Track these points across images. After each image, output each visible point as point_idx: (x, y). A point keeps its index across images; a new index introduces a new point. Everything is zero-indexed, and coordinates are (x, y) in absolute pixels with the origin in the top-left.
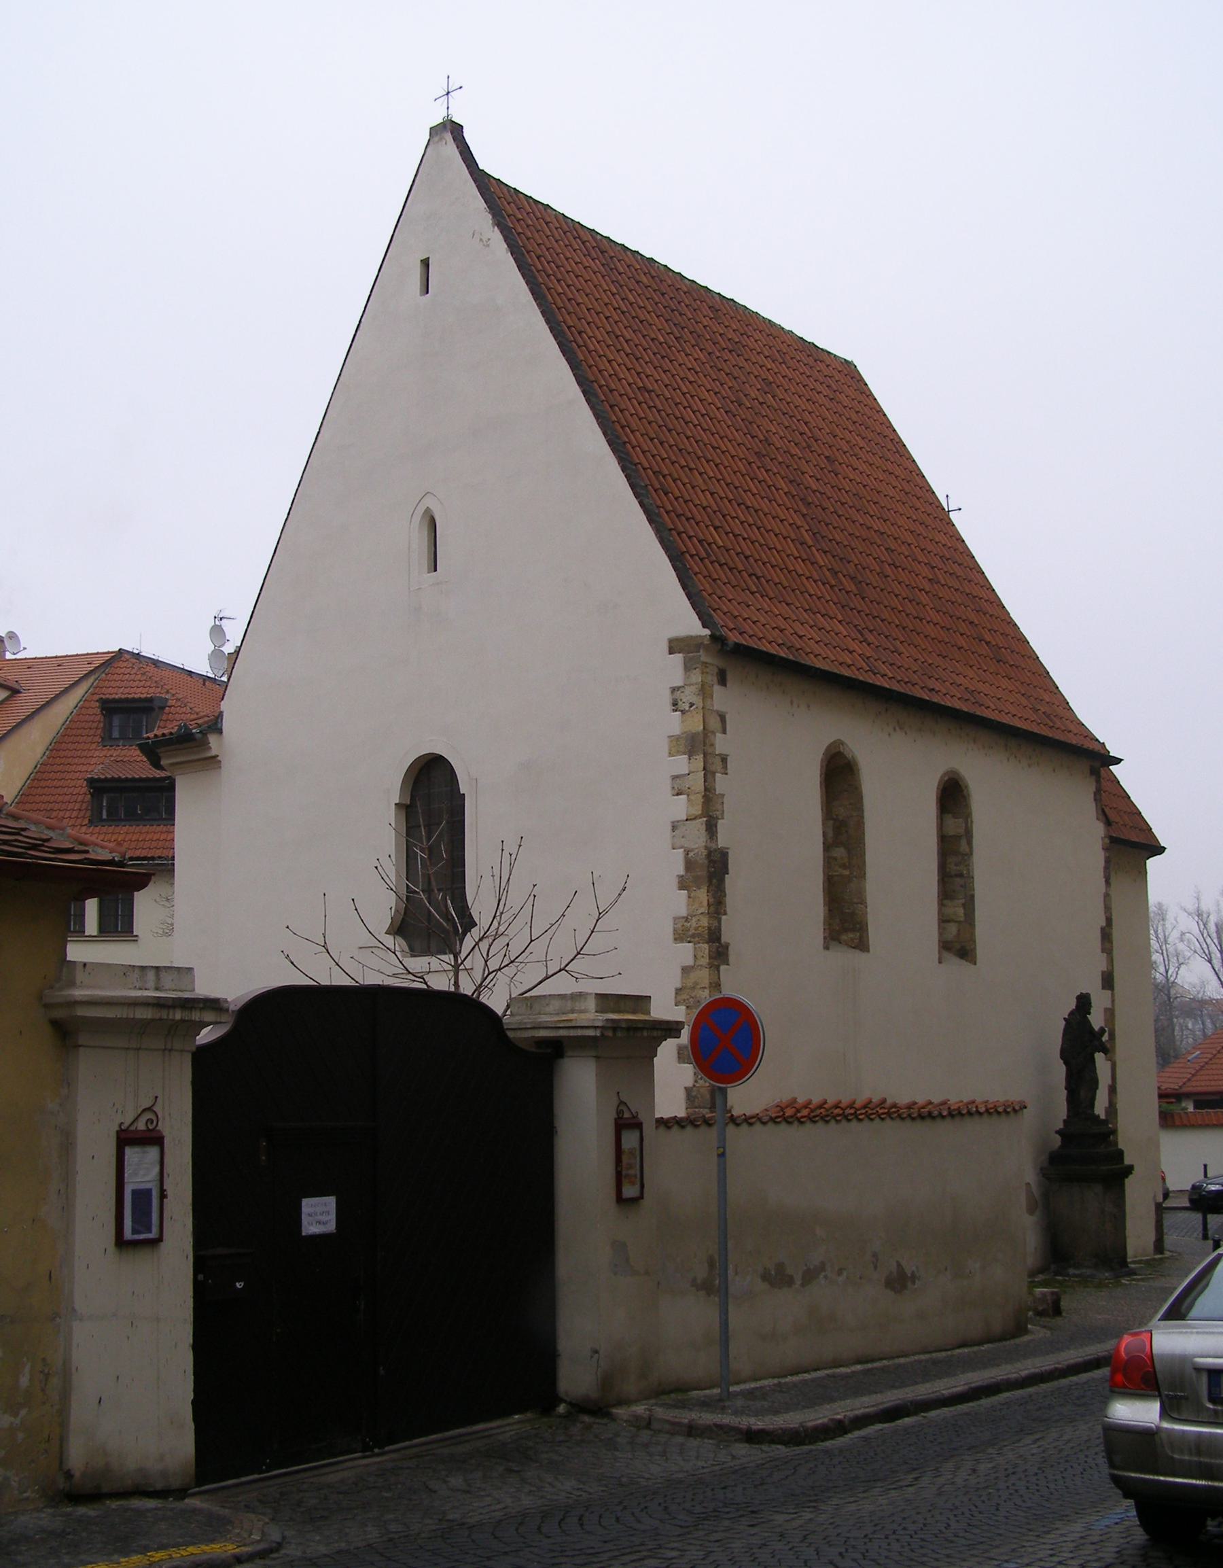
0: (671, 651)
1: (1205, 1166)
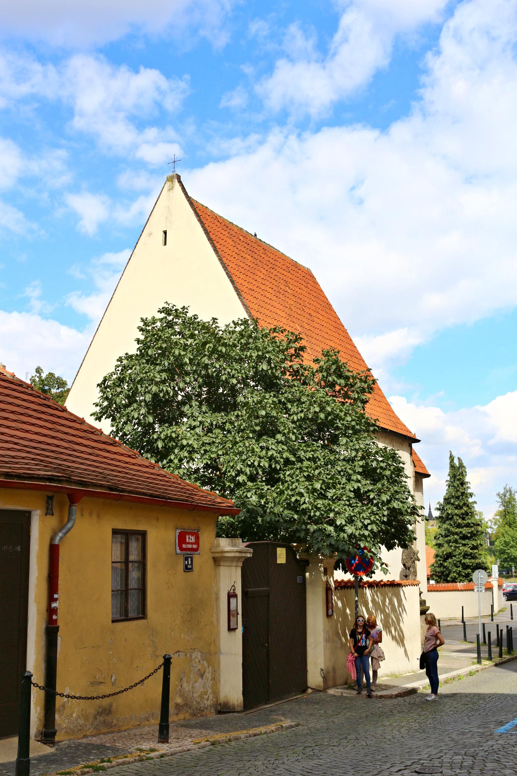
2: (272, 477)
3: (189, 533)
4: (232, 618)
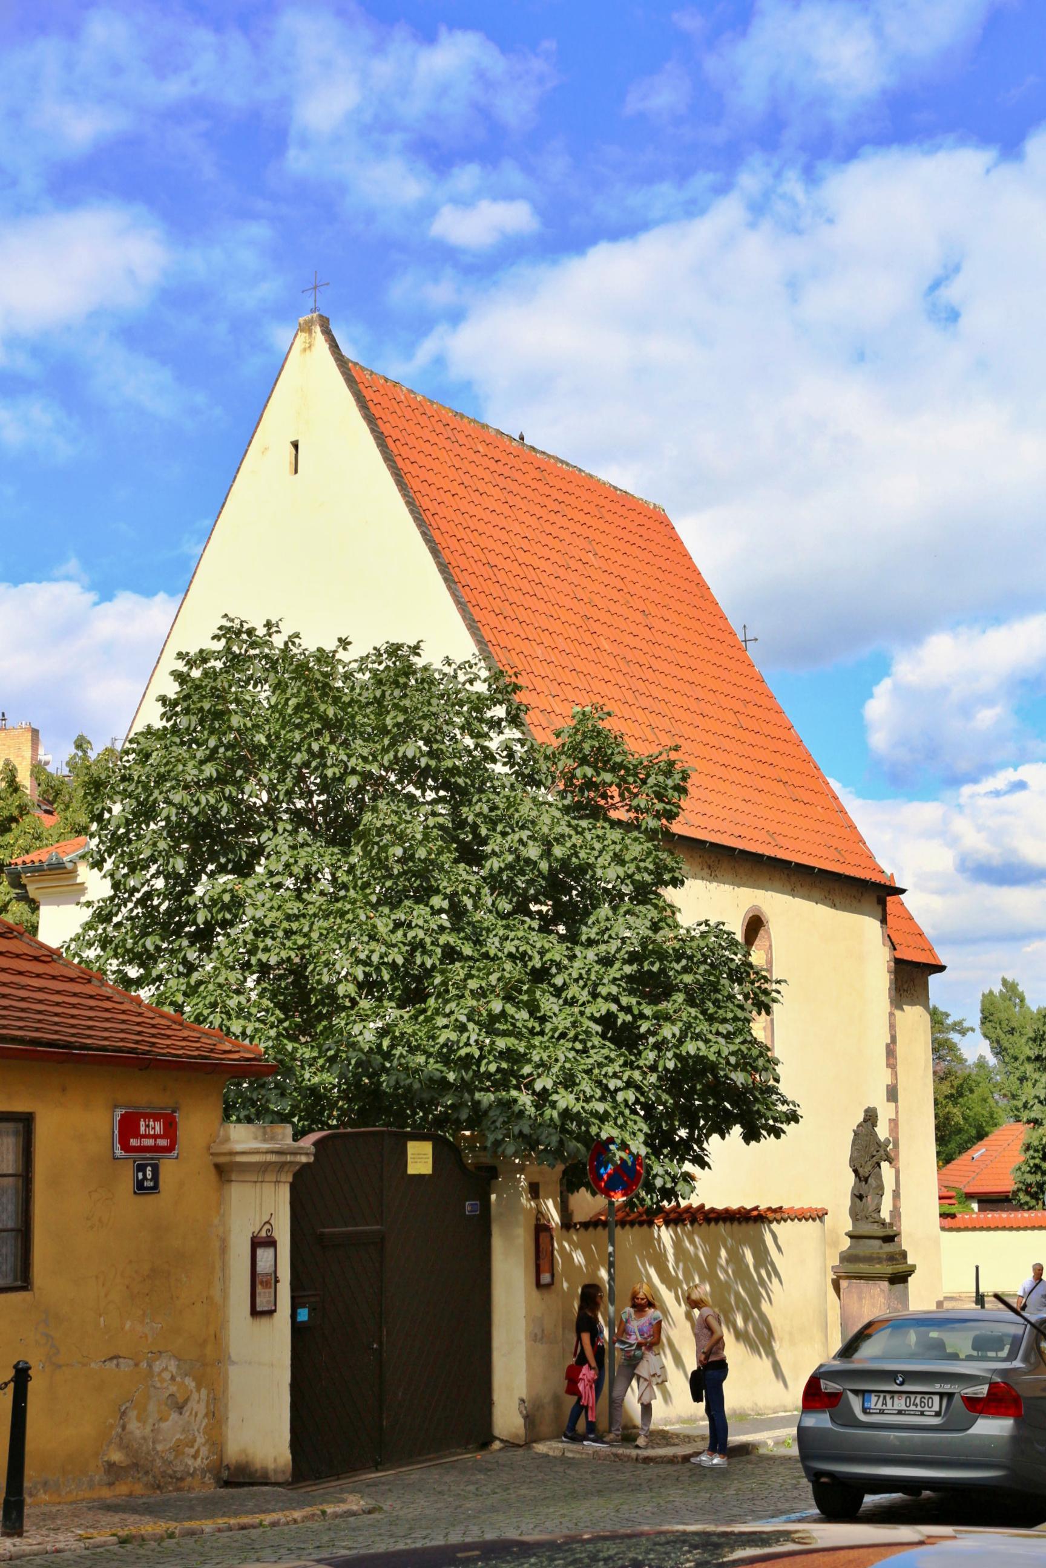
1: (977, 1268)
2: (413, 991)
3: (147, 1116)
4: (259, 1289)
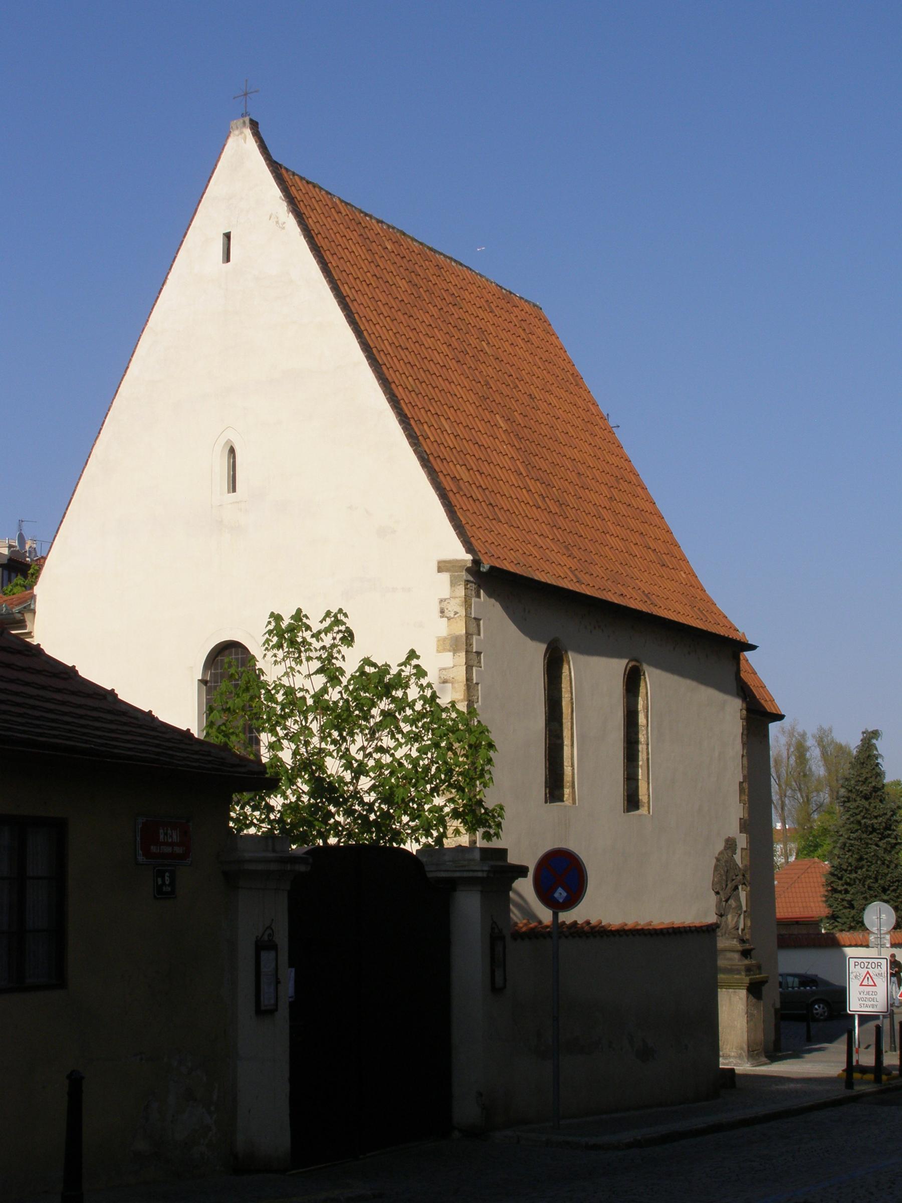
0: (440, 570)
